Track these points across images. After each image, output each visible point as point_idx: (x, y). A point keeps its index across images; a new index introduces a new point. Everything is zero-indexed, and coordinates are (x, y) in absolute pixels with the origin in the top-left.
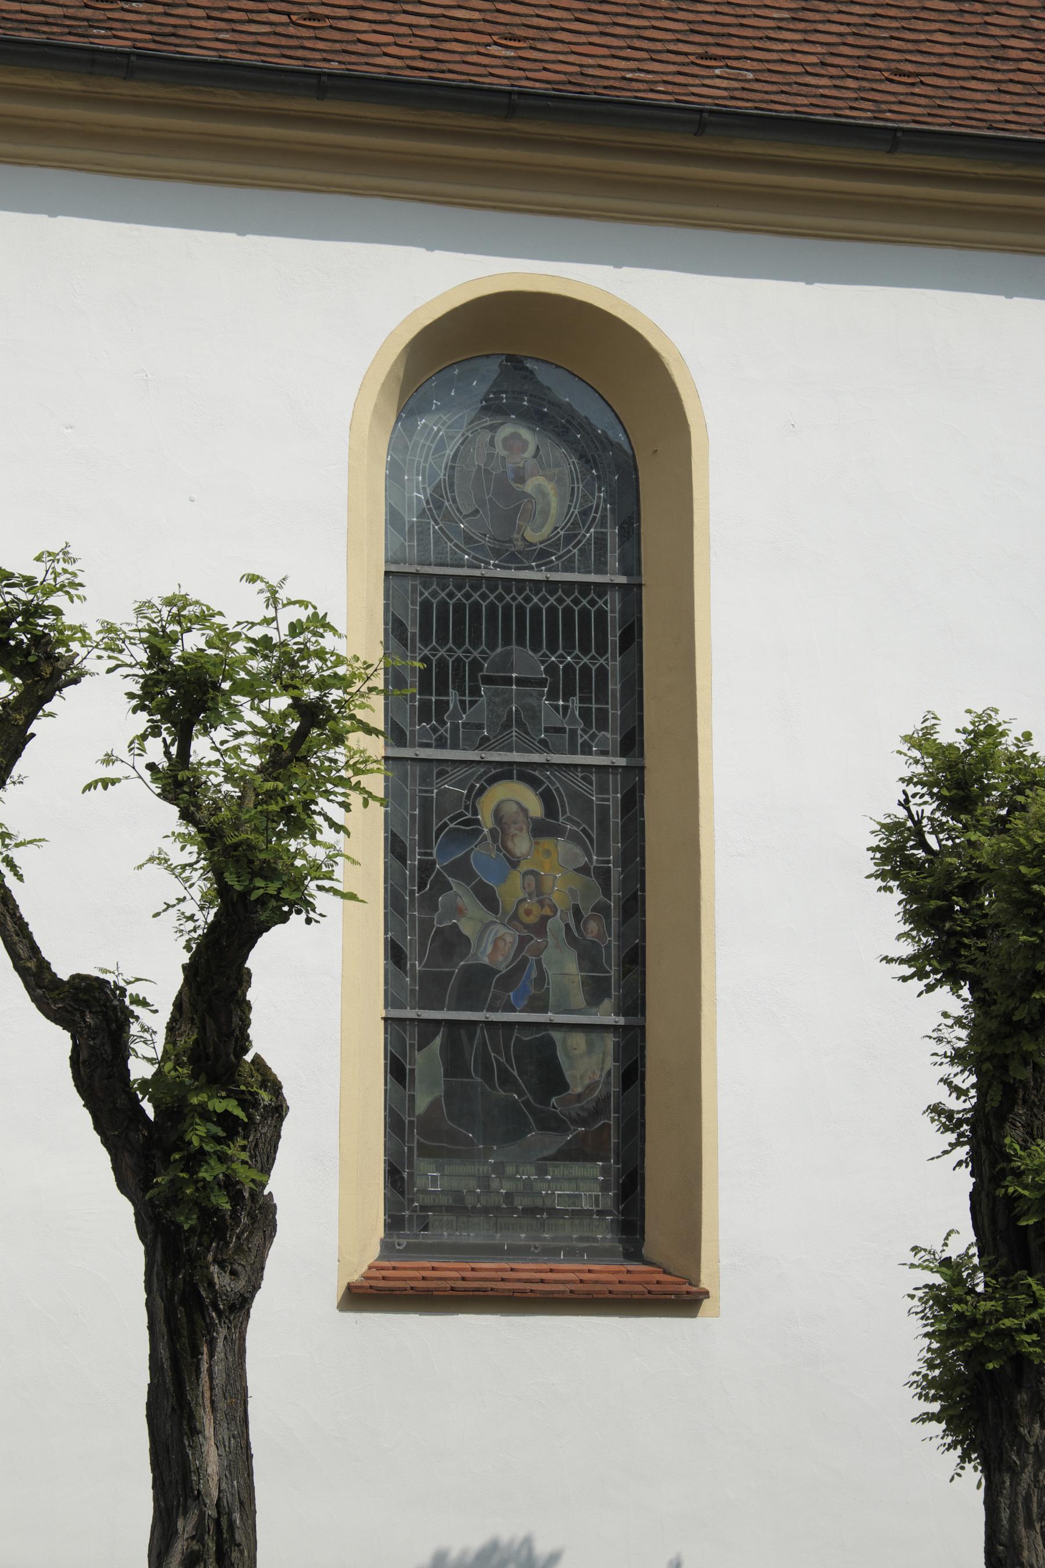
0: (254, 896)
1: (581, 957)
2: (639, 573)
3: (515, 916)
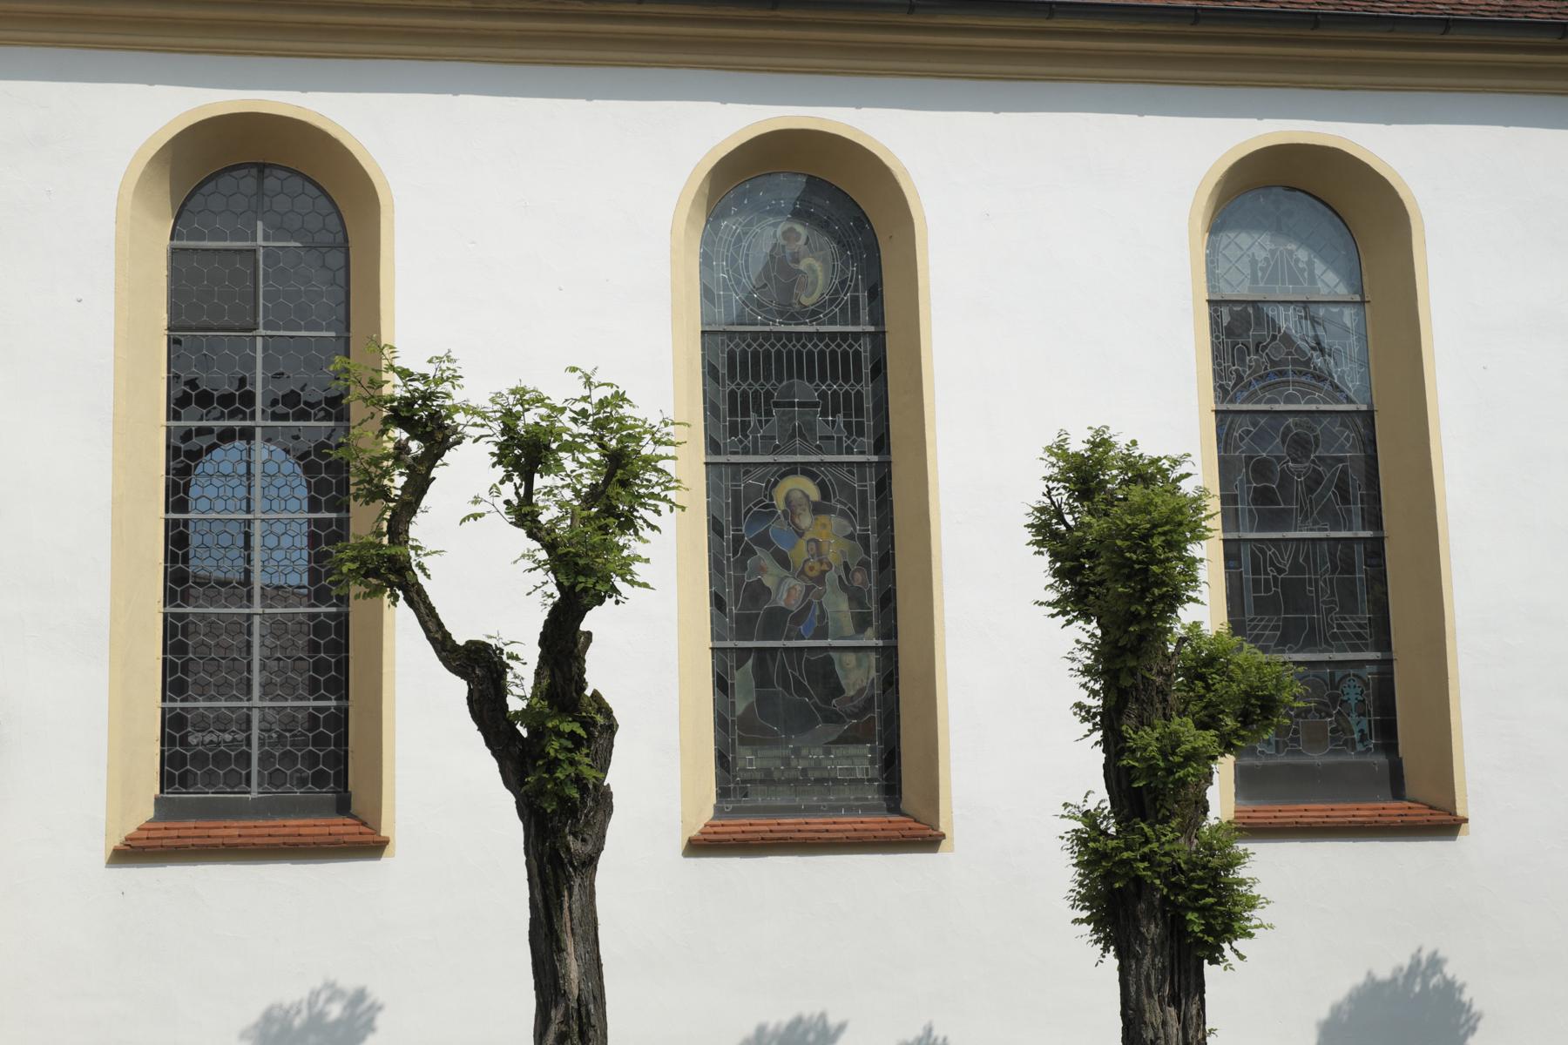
0: (578, 589)
1: (850, 599)
2: (883, 324)
3: (802, 572)
